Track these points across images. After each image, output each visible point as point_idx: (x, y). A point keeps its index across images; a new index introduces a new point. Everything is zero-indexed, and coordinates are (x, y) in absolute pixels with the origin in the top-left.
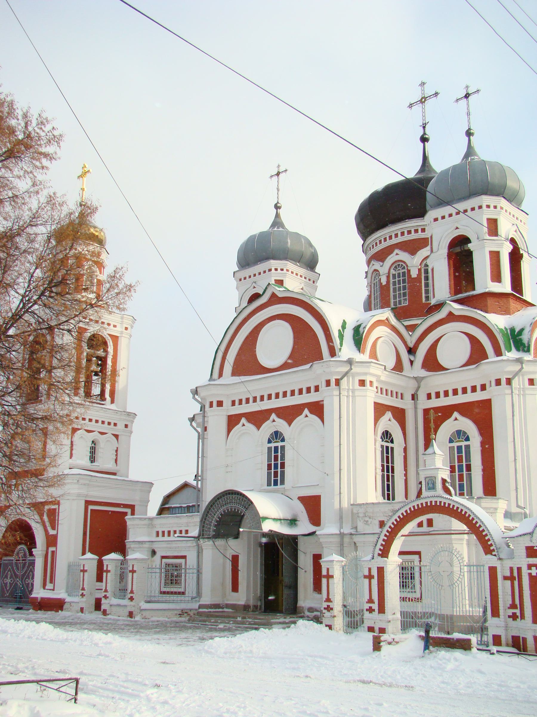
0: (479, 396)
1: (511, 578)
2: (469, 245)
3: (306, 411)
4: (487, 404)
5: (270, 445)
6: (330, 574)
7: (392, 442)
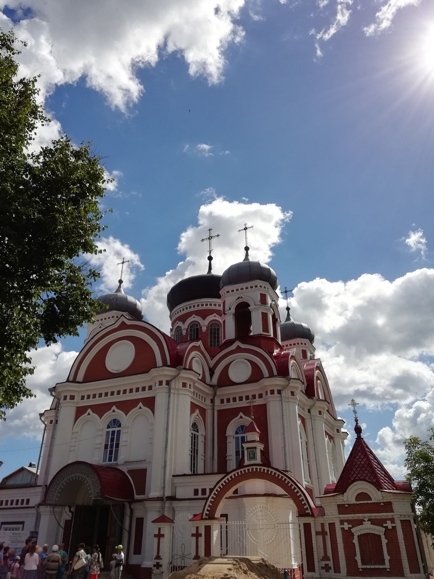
0: (258, 402)
1: (323, 533)
2: (249, 308)
3: (141, 404)
4: (263, 408)
5: (109, 430)
6: (162, 533)
7: (198, 431)
